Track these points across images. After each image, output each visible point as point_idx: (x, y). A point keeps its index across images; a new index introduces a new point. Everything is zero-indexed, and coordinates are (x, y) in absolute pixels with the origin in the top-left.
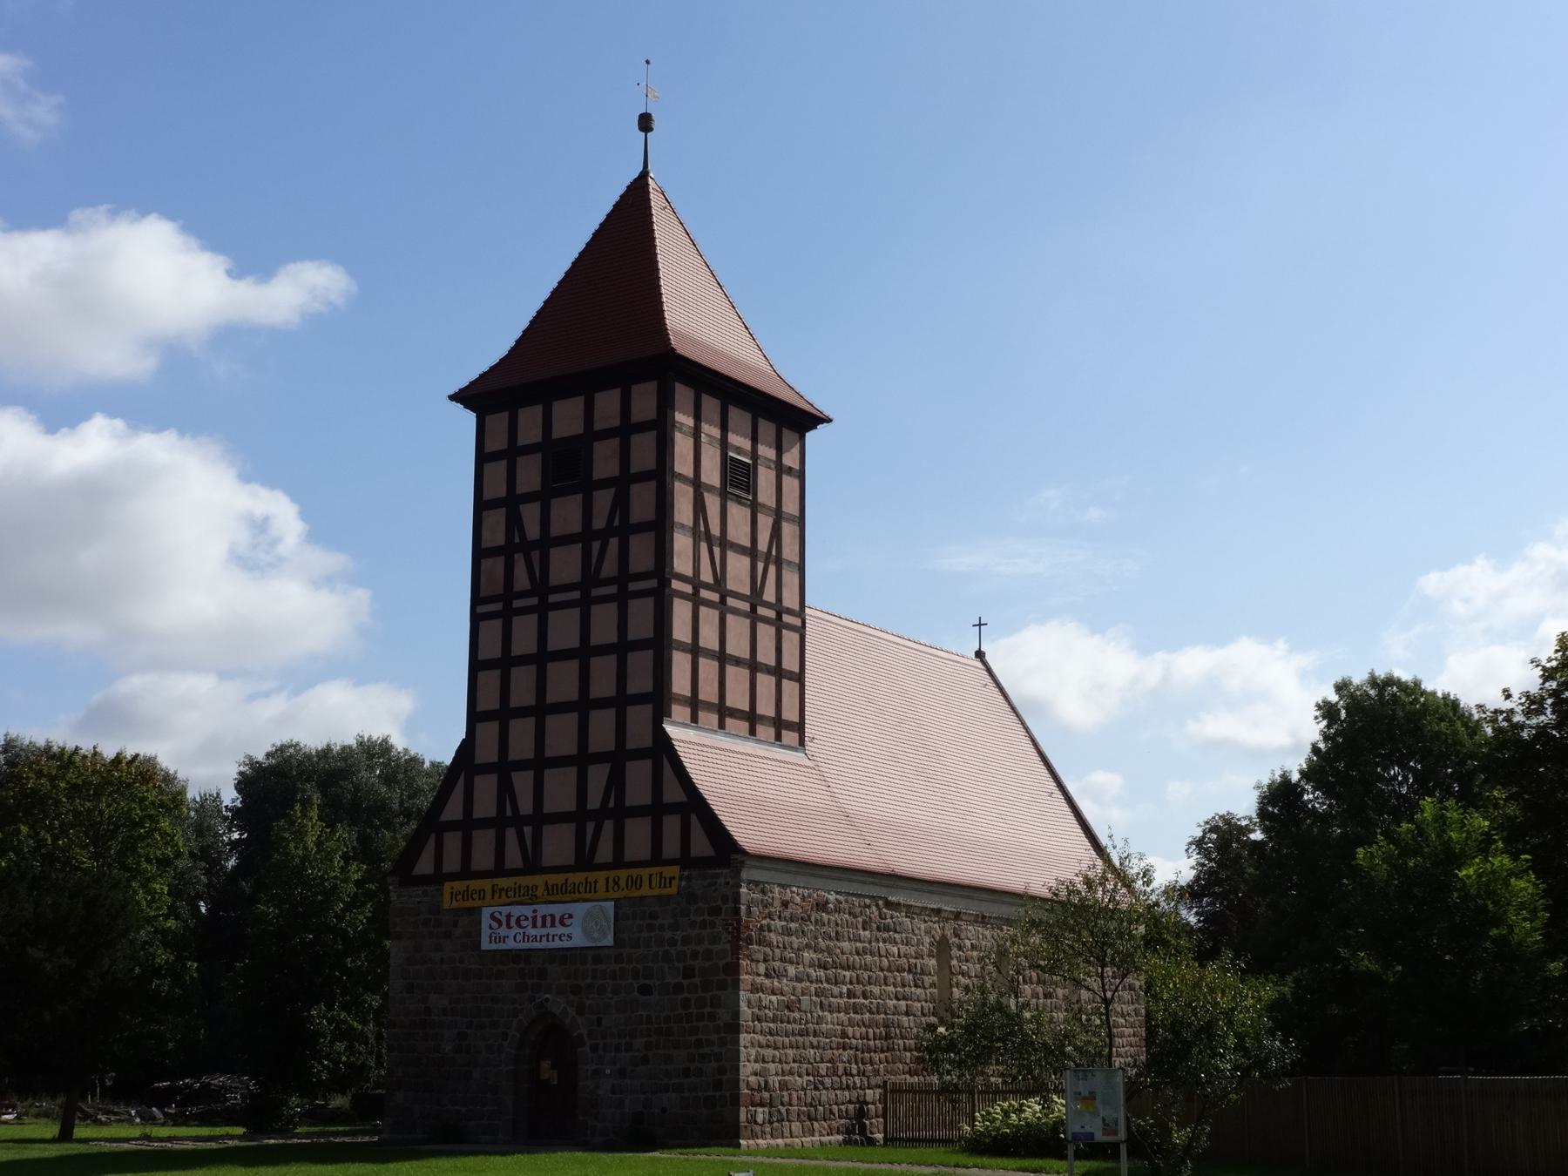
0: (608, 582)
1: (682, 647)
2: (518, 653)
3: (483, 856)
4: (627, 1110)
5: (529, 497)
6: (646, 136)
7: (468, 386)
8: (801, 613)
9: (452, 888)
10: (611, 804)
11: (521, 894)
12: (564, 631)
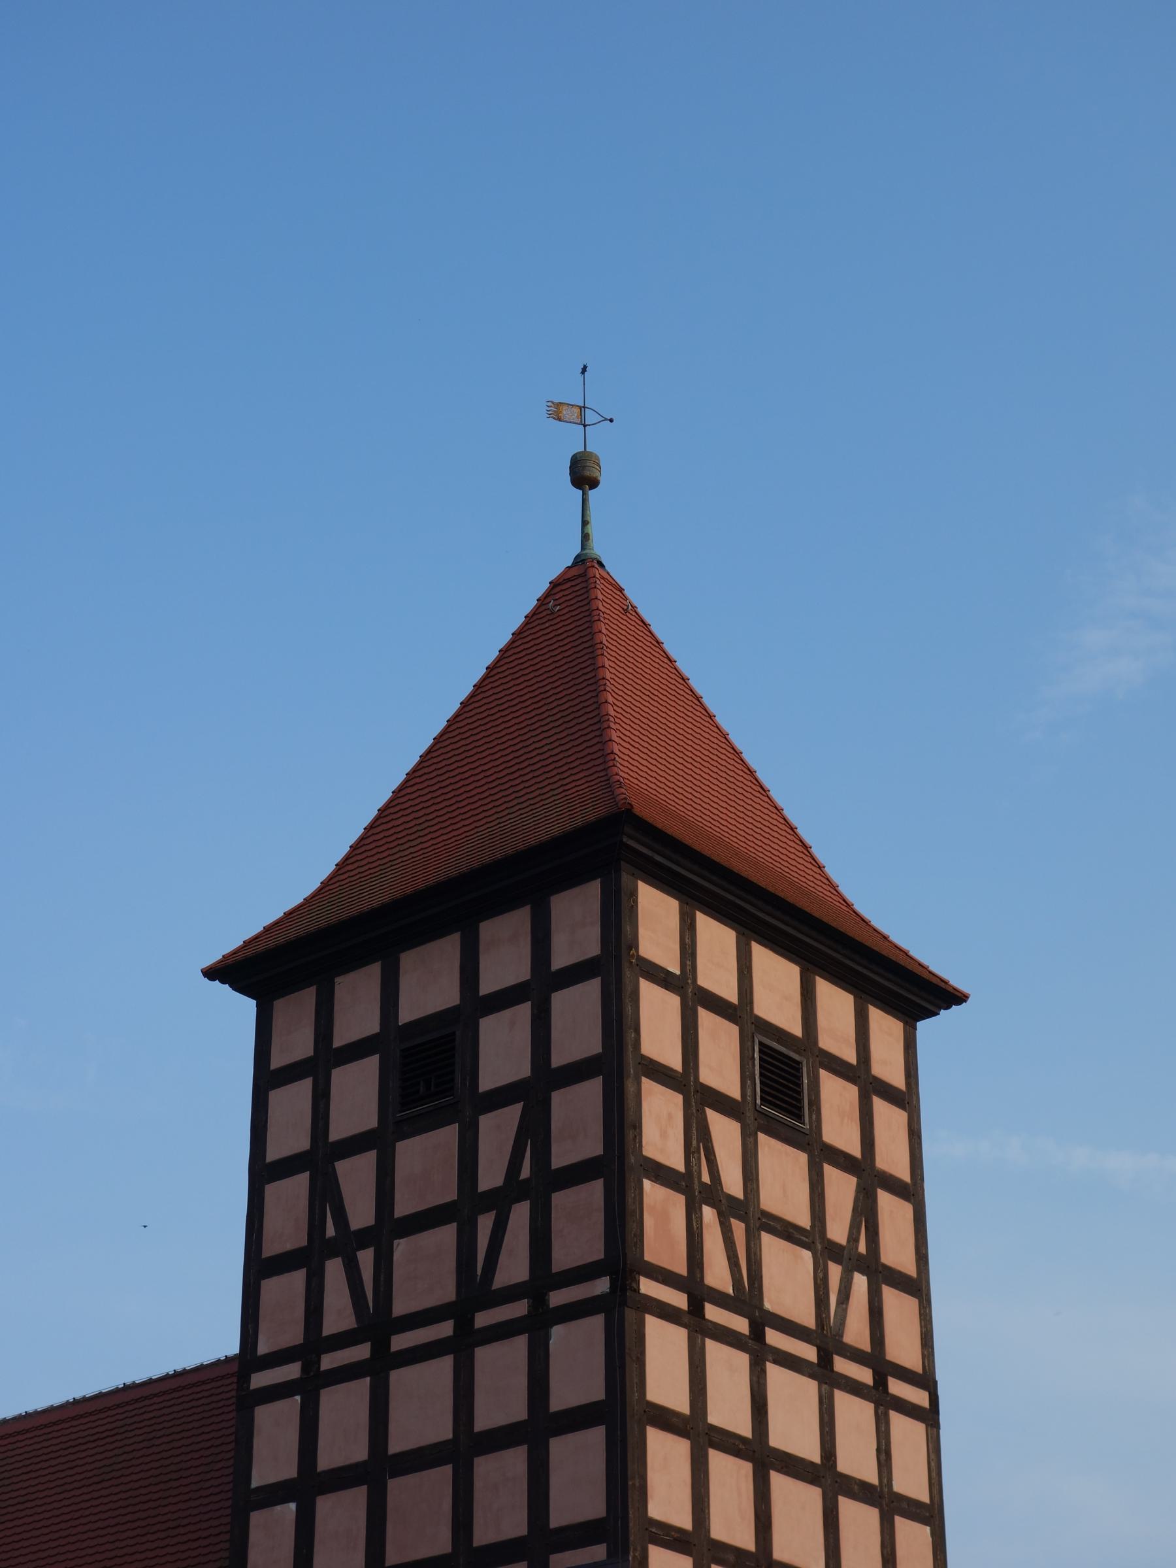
0: (510, 1294)
2: (326, 1468)
5: (354, 1145)
6: (585, 501)
8: (926, 1380)
10: (525, 1173)
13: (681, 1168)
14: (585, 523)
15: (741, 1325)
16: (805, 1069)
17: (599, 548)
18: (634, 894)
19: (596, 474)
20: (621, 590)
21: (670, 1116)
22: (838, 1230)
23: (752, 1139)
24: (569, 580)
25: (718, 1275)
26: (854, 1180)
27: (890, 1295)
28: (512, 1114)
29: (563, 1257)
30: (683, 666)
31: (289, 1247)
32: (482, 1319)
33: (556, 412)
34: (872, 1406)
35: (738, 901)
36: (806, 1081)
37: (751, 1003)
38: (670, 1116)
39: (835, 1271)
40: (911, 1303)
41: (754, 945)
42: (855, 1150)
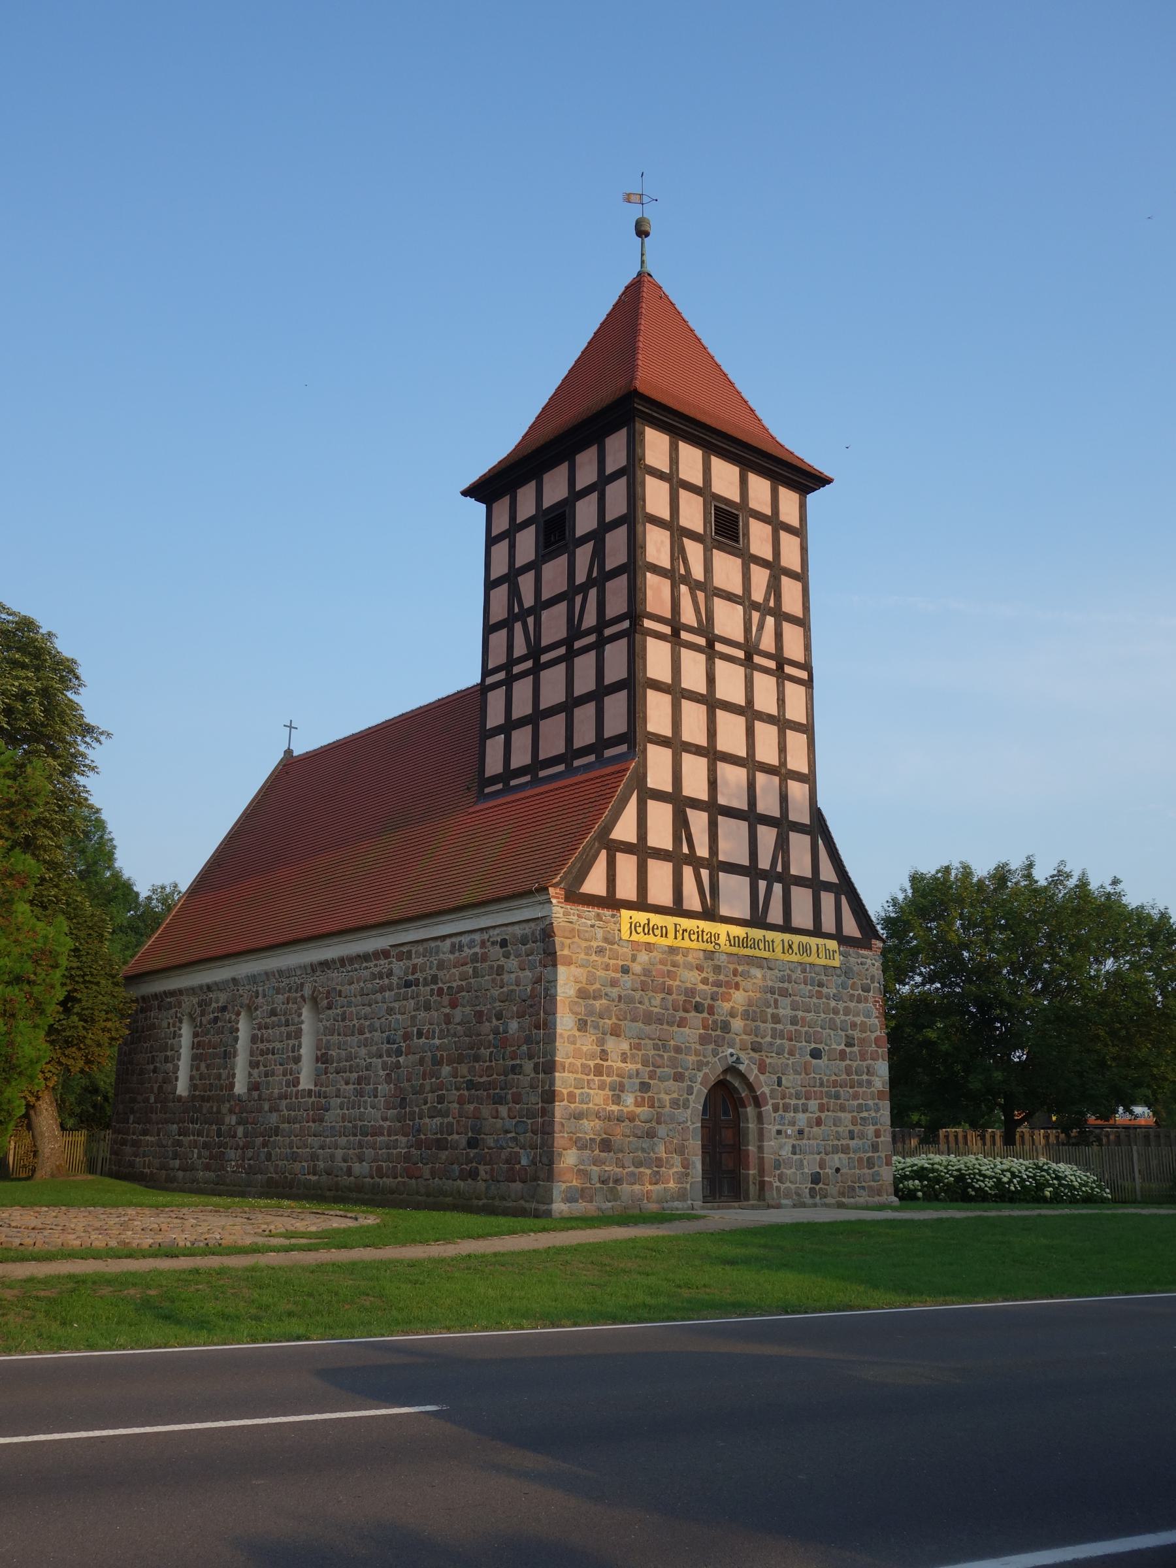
0: (588, 632)
1: (657, 686)
3: (660, 891)
4: (806, 1170)
6: (642, 244)
7: (593, 338)
8: (807, 666)
9: (631, 918)
10: (595, 574)
11: (705, 939)
12: (553, 687)
13: (668, 567)
14: (642, 255)
15: (702, 641)
16: (741, 518)
17: (649, 268)
18: (643, 433)
19: (648, 229)
20: (660, 288)
21: (662, 542)
23: (709, 553)
24: (633, 285)
25: (688, 616)
26: (768, 571)
27: (787, 627)
28: (589, 546)
29: (610, 613)
30: (692, 324)
31: (500, 618)
33: (628, 198)
34: (775, 678)
35: (701, 435)
36: (741, 524)
37: (710, 486)
38: (662, 542)
39: (756, 616)
41: (712, 457)
42: (769, 557)
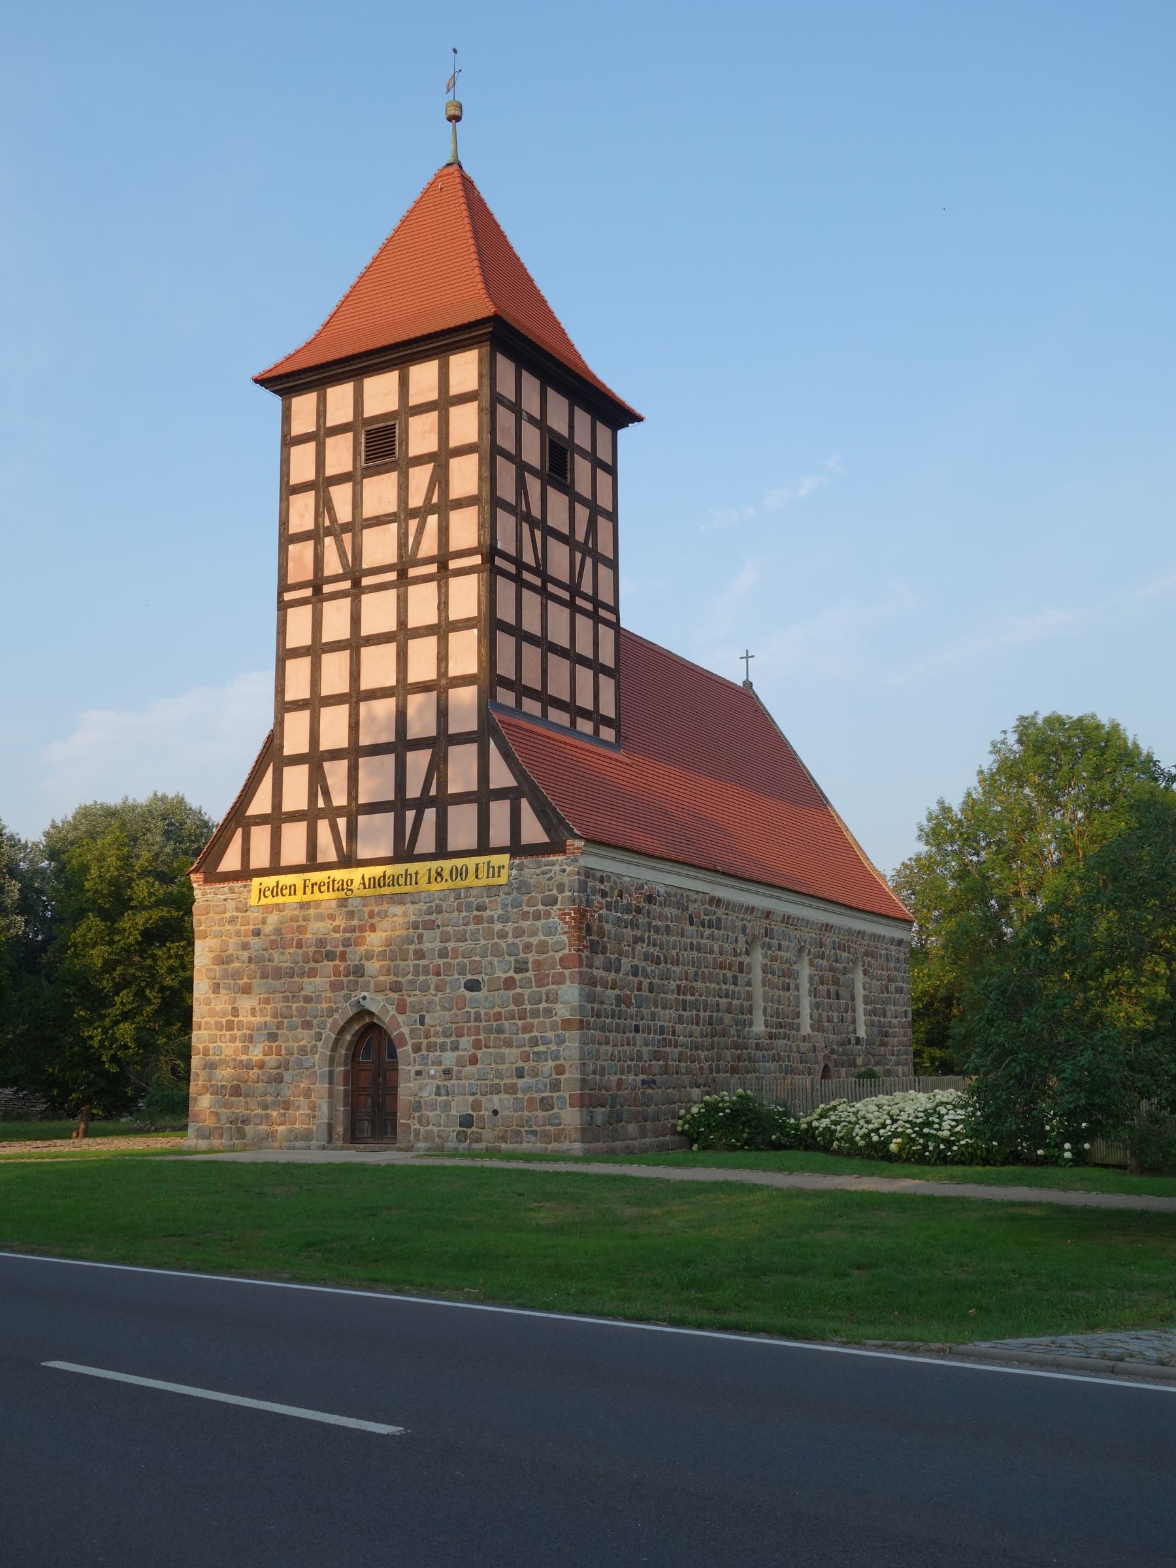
0: (428, 561)
8: (615, 610)
10: (435, 500)
22: (580, 536)
32: (413, 572)
39: (578, 556)
40: (609, 479)
42: (589, 449)
